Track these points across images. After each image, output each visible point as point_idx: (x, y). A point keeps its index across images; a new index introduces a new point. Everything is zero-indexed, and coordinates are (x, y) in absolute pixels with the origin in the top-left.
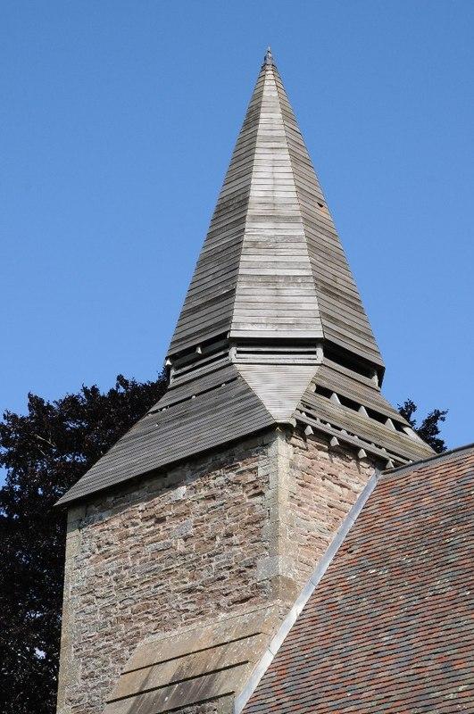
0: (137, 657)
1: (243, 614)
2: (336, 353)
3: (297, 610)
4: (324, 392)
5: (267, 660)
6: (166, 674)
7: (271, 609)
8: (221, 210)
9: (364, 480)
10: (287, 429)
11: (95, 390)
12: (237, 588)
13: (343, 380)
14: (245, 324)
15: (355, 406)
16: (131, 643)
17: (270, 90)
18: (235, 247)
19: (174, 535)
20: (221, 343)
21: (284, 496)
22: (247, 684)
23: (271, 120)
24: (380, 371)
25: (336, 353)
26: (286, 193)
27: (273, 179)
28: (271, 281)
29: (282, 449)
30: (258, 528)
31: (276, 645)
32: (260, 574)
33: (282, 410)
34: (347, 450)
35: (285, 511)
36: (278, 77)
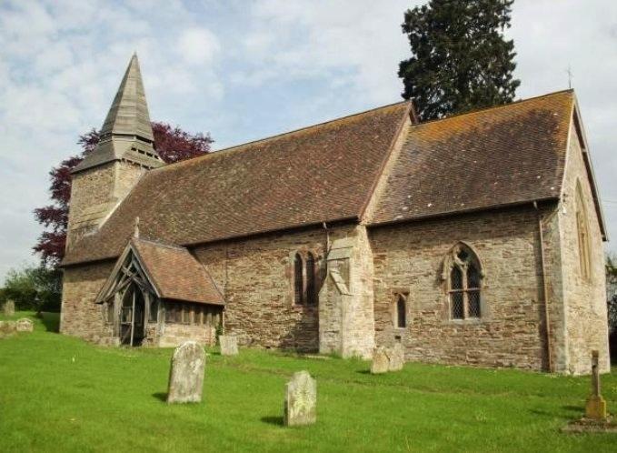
4: (134, 149)
10: (119, 160)
30: (111, 183)
32: (110, 196)
34: (137, 165)
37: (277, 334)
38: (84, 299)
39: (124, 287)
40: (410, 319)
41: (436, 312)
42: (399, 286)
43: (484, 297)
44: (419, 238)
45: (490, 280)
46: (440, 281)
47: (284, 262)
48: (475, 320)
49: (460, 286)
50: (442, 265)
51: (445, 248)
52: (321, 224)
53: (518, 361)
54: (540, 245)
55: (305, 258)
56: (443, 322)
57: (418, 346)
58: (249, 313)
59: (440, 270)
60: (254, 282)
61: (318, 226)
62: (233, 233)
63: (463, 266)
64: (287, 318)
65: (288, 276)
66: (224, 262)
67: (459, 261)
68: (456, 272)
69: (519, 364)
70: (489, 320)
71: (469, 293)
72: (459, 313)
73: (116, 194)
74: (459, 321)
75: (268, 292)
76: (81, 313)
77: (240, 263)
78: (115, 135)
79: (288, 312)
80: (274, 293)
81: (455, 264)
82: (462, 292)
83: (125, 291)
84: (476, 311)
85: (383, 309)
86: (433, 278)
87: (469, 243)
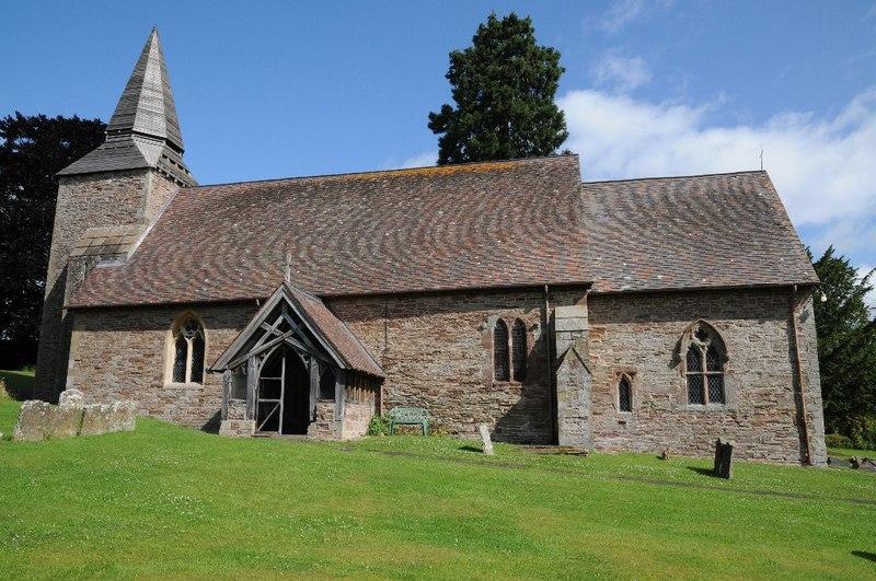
1: (131, 227)
2: (169, 143)
4: (165, 157)
6: (101, 241)
7: (142, 227)
8: (132, 81)
9: (174, 189)
10: (153, 169)
12: (129, 218)
13: (171, 152)
15: (174, 163)
16: (84, 228)
17: (155, 40)
18: (137, 97)
19: (105, 195)
21: (149, 191)
23: (154, 52)
24: (183, 152)
26: (158, 81)
27: (153, 74)
28: (149, 113)
29: (151, 176)
30: (139, 200)
31: (142, 239)
32: (138, 215)
33: (152, 163)
34: (171, 179)
35: (149, 196)
37: (469, 416)
38: (116, 358)
39: (266, 351)
40: (636, 402)
41: (670, 396)
42: (622, 363)
43: (728, 381)
44: (647, 312)
45: (735, 363)
46: (676, 361)
47: (481, 329)
48: (719, 405)
49: (700, 369)
50: (679, 345)
51: (681, 326)
52: (542, 287)
53: (770, 452)
54: (794, 331)
55: (511, 326)
56: (680, 408)
57: (647, 433)
58: (425, 390)
59: (678, 349)
60: (432, 350)
61: (539, 288)
62: (395, 285)
63: (703, 347)
64: (485, 397)
65: (486, 346)
66: (381, 321)
67: (697, 341)
68: (694, 350)
69: (773, 456)
70: (735, 407)
71: (708, 376)
72: (696, 395)
73: (147, 214)
74: (699, 406)
75: (453, 363)
76: (110, 378)
77: (408, 324)
78: (136, 133)
79: (487, 390)
80: (464, 366)
81: (693, 344)
82: (702, 375)
83: (266, 357)
84: (719, 396)
85: (602, 390)
86: (669, 357)
87: (711, 323)
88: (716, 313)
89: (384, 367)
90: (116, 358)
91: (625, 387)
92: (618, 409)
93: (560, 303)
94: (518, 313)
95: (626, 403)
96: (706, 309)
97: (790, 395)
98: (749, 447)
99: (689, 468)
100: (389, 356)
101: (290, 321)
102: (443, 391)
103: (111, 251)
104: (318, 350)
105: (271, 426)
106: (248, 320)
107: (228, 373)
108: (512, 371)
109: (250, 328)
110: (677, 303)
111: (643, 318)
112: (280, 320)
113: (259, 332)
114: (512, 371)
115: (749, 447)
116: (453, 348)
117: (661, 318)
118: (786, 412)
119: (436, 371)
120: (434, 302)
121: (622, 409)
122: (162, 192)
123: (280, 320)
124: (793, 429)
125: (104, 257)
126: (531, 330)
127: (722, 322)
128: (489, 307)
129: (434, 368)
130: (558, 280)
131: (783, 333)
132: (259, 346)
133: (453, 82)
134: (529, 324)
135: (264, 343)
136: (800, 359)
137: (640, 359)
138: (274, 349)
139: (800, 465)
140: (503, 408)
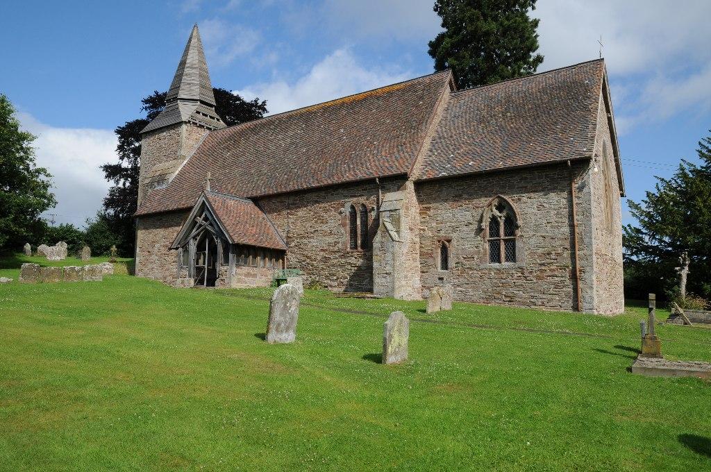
0: (154, 168)
2: (202, 102)
3: (185, 162)
4: (198, 112)
5: (177, 172)
6: (158, 174)
9: (205, 133)
10: (186, 123)
11: (431, 42)
14: (182, 95)
15: (206, 116)
20: (176, 99)
22: (171, 178)
25: (202, 102)
29: (184, 127)
34: (201, 126)
36: (235, 90)
37: (334, 275)
39: (198, 235)
40: (452, 263)
42: (442, 234)
43: (519, 244)
46: (480, 230)
48: (510, 264)
49: (498, 235)
51: (484, 201)
55: (359, 209)
56: (482, 267)
61: (371, 181)
63: (500, 217)
64: (343, 261)
65: (344, 225)
67: (497, 213)
68: (494, 221)
70: (524, 265)
72: (495, 257)
73: (183, 152)
74: (497, 265)
79: (343, 256)
80: (331, 240)
84: (512, 257)
85: (427, 254)
86: (475, 226)
87: (506, 197)
88: (512, 189)
89: (287, 244)
90: (157, 245)
91: (445, 251)
92: (439, 268)
93: (389, 190)
94: (362, 200)
95: (445, 265)
96: (504, 187)
97: (567, 254)
98: (533, 297)
99: (419, 311)
100: (290, 235)
101: (209, 215)
102: (319, 258)
103: (161, 179)
104: (220, 234)
105: (201, 282)
106: (187, 218)
107: (180, 249)
108: (359, 242)
109: (189, 221)
110: (483, 183)
111: (457, 198)
112: (203, 216)
113: (194, 223)
114: (359, 242)
115: (533, 297)
116: (325, 228)
117: (471, 196)
118: (564, 268)
119: (315, 244)
120: (313, 196)
121: (442, 268)
122: (195, 136)
123: (203, 216)
124: (568, 282)
125: (158, 182)
126: (370, 212)
127: (516, 197)
128: (346, 197)
129: (314, 242)
130: (387, 173)
131: (565, 201)
132: (194, 232)
133: (440, 14)
134: (369, 206)
135: (197, 229)
136: (576, 222)
137: (454, 229)
138: (202, 233)
139: (571, 312)
140: (353, 268)
